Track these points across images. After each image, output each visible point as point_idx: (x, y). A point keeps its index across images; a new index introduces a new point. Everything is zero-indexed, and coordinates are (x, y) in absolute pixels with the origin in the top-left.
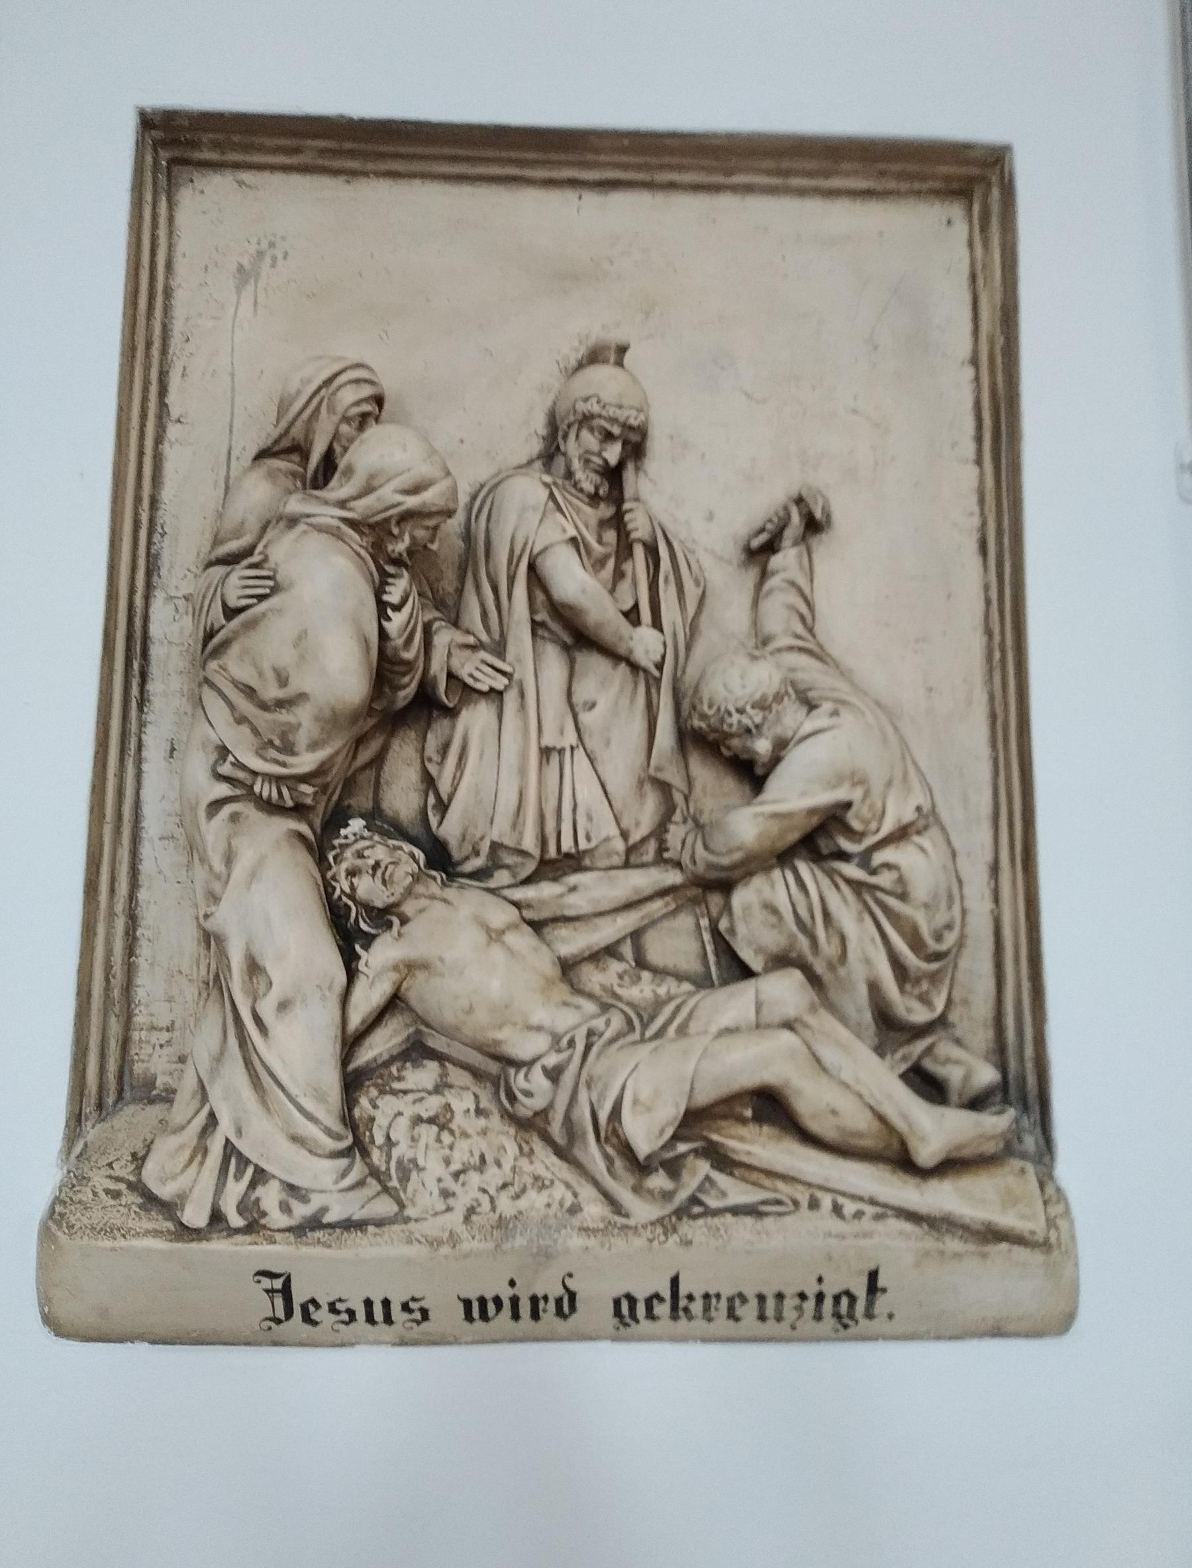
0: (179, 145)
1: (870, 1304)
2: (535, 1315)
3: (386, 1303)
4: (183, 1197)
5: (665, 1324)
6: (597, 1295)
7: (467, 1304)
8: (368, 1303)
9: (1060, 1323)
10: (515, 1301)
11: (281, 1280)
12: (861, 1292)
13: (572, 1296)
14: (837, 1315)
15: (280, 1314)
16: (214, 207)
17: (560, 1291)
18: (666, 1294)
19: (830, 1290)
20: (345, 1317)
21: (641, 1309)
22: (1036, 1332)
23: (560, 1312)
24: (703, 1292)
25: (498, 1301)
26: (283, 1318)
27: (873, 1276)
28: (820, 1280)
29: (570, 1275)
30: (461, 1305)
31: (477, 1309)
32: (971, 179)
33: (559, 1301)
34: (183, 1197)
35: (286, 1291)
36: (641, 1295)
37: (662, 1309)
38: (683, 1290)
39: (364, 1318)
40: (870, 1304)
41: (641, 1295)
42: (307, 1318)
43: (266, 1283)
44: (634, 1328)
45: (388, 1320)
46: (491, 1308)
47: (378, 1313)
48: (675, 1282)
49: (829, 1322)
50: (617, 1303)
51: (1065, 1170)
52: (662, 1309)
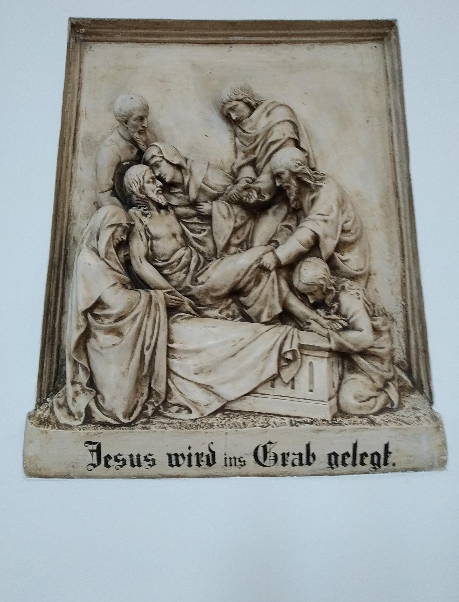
0: (85, 32)
1: (386, 457)
2: (199, 465)
3: (138, 456)
4: (382, 377)
5: (194, 469)
6: (321, 452)
7: (170, 456)
8: (131, 456)
9: (441, 464)
10: (190, 455)
11: (97, 445)
12: (382, 452)
13: (213, 453)
14: (372, 463)
15: (95, 462)
16: (100, 56)
17: (208, 452)
18: (351, 453)
19: (193, 452)
20: (151, 463)
21: (340, 459)
22: (431, 468)
23: (209, 464)
24: (196, 452)
25: (182, 455)
26: (96, 464)
27: (387, 446)
28: (190, 448)
29: (212, 443)
30: (167, 456)
31: (174, 460)
32: (382, 32)
33: (208, 456)
34: (382, 377)
35: (98, 451)
36: (340, 452)
37: (349, 460)
38: (360, 451)
39: (129, 464)
40: (386, 457)
41: (340, 452)
42: (107, 466)
43: (90, 447)
44: (337, 469)
45: (139, 465)
46: (181, 459)
47: (135, 461)
48: (387, 446)
49: (369, 466)
50: (330, 455)
51: (439, 406)
52: (349, 460)
